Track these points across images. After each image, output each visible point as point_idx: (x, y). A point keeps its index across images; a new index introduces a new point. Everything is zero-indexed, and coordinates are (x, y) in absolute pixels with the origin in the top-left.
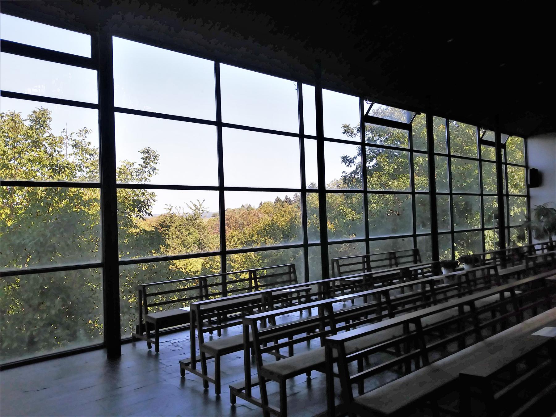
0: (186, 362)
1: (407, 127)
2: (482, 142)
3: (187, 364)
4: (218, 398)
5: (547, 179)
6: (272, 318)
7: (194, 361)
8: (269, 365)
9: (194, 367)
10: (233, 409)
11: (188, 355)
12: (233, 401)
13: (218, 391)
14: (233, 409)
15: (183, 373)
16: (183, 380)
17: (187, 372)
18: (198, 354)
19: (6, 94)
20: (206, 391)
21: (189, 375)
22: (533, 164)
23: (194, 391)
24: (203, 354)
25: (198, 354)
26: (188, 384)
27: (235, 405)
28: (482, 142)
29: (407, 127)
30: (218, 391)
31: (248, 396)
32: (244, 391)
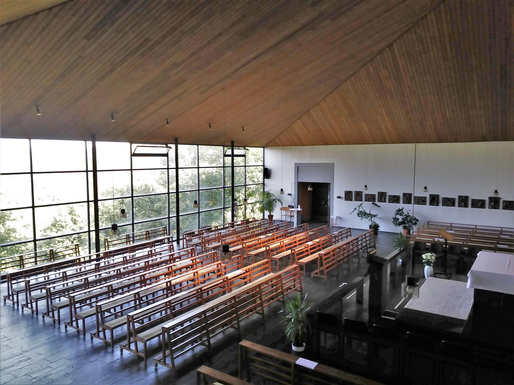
0: (6, 296)
1: (166, 155)
2: (225, 155)
3: (6, 297)
4: (18, 308)
5: (273, 175)
6: (67, 284)
7: (9, 295)
8: (15, 288)
9: (9, 298)
10: (23, 311)
11: (7, 294)
12: (23, 309)
13: (18, 306)
14: (23, 311)
15: (5, 300)
16: (5, 303)
17: (6, 300)
18: (10, 293)
19: (2, 174)
20: (14, 307)
21: (8, 301)
22: (268, 165)
23: (9, 306)
24: (12, 293)
25: (10, 293)
26: (7, 304)
27: (157, 367)
28: (225, 155)
29: (166, 155)
30: (18, 306)
31: (129, 349)
32: (127, 346)
